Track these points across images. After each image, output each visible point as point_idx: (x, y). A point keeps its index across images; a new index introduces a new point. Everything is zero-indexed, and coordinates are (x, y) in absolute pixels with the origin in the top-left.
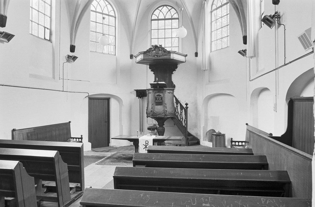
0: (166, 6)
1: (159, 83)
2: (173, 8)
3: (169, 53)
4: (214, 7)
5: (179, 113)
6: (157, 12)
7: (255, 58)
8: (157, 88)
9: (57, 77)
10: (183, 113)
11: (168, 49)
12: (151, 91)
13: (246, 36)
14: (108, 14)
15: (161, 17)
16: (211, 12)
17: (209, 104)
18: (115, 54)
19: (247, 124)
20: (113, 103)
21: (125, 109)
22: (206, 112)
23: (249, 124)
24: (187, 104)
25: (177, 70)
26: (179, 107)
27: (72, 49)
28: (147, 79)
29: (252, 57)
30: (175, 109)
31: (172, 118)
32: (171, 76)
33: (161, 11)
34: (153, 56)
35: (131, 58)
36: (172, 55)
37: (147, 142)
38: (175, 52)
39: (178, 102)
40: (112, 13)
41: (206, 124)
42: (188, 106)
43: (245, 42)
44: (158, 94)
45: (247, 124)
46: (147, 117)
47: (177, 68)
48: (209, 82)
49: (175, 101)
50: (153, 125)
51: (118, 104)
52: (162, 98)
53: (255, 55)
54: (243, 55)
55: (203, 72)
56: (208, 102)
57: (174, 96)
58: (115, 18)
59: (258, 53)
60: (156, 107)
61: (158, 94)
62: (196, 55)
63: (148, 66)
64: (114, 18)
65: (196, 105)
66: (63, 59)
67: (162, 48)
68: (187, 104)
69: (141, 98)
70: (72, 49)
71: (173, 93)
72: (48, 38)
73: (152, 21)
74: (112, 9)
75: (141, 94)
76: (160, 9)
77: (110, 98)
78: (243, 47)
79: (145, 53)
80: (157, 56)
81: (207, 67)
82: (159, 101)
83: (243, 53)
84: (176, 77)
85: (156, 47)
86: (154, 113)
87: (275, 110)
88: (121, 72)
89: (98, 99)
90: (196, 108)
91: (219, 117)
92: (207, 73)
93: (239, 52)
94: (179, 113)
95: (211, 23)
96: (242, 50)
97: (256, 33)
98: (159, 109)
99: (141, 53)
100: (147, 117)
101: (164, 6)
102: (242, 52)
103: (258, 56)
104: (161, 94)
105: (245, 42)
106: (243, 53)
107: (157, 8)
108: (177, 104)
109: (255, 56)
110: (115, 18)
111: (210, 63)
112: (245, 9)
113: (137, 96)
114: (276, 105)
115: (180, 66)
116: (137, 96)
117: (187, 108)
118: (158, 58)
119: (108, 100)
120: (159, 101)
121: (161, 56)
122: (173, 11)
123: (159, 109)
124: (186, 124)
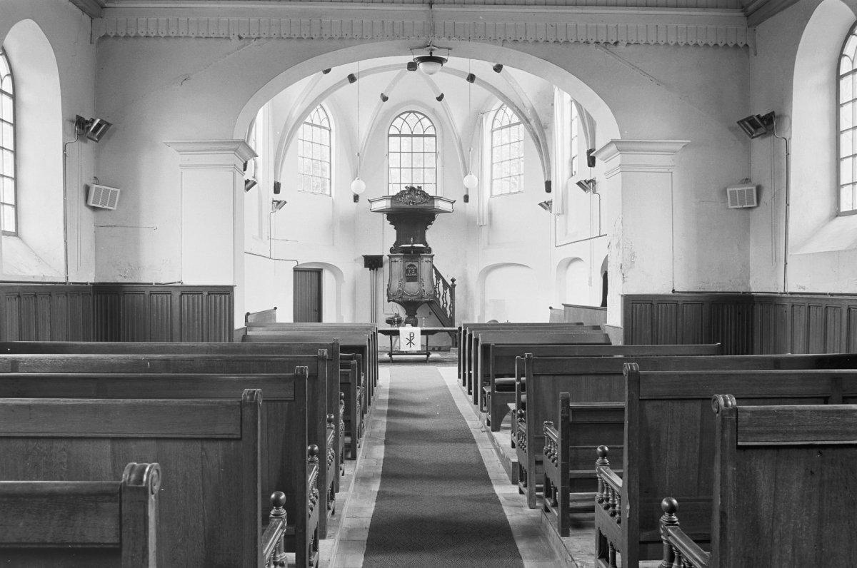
0: (414, 112)
1: (415, 245)
2: (425, 116)
3: (432, 198)
4: (497, 125)
5: (442, 294)
6: (398, 122)
7: (562, 217)
8: (410, 252)
9: (265, 237)
10: (448, 294)
11: (431, 193)
12: (397, 259)
13: (550, 182)
14: (319, 124)
15: (406, 131)
16: (492, 131)
17: (487, 279)
18: (331, 195)
19: (551, 308)
20: (327, 278)
21: (346, 289)
22: (483, 293)
23: (553, 308)
24: (453, 280)
25: (434, 223)
26: (441, 285)
27: (277, 189)
28: (384, 239)
29: (559, 214)
30: (435, 287)
31: (430, 303)
32: (425, 233)
33: (404, 120)
34: (407, 204)
35: (355, 201)
36: (436, 201)
37: (412, 335)
38: (440, 198)
39: (439, 276)
40: (325, 124)
41: (483, 311)
42: (455, 283)
43: (548, 189)
44: (410, 263)
45: (551, 308)
46: (389, 301)
47: (434, 219)
48: (489, 244)
49: (434, 275)
50: (393, 316)
51: (333, 276)
52: (416, 270)
53: (564, 211)
54: (546, 209)
55: (475, 227)
56: (486, 276)
57: (434, 267)
58: (330, 130)
59: (567, 210)
60: (407, 284)
61: (410, 263)
62: (466, 199)
63: (385, 216)
64: (328, 132)
65: (465, 279)
66: (268, 205)
67: (421, 191)
68: (453, 280)
69: (373, 270)
70: (277, 189)
71: (431, 262)
72: (328, 193)
73: (390, 138)
74: (325, 116)
75: (373, 263)
76: (404, 116)
77: (322, 269)
78: (547, 197)
79: (393, 198)
80: (413, 203)
81: (486, 221)
82: (411, 276)
83: (546, 205)
84: (433, 235)
85: (412, 189)
86: (404, 294)
87: (590, 284)
88: (348, 226)
89: (305, 271)
90: (466, 287)
91: (504, 300)
92: (485, 230)
93: (540, 204)
94: (442, 294)
95: (492, 150)
96: (545, 202)
97: (565, 183)
98: (412, 287)
99: (385, 198)
100: (389, 301)
101: (410, 112)
102: (545, 205)
103: (567, 214)
104: (414, 263)
105: (548, 189)
106: (546, 205)
107: (399, 116)
108: (438, 279)
109: (563, 213)
110: (330, 130)
111: (490, 214)
112: (549, 143)
113: (366, 266)
114: (591, 278)
115: (438, 217)
116: (366, 266)
117: (454, 286)
118: (415, 206)
119: (319, 272)
120: (411, 276)
121: (419, 203)
122: (426, 122)
123: (412, 287)
124: (453, 312)
